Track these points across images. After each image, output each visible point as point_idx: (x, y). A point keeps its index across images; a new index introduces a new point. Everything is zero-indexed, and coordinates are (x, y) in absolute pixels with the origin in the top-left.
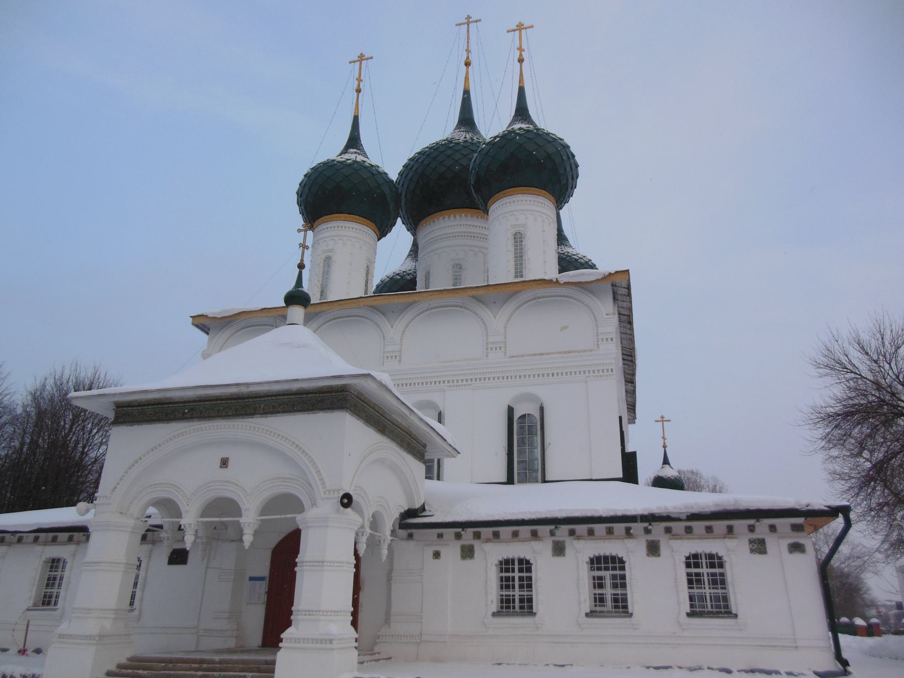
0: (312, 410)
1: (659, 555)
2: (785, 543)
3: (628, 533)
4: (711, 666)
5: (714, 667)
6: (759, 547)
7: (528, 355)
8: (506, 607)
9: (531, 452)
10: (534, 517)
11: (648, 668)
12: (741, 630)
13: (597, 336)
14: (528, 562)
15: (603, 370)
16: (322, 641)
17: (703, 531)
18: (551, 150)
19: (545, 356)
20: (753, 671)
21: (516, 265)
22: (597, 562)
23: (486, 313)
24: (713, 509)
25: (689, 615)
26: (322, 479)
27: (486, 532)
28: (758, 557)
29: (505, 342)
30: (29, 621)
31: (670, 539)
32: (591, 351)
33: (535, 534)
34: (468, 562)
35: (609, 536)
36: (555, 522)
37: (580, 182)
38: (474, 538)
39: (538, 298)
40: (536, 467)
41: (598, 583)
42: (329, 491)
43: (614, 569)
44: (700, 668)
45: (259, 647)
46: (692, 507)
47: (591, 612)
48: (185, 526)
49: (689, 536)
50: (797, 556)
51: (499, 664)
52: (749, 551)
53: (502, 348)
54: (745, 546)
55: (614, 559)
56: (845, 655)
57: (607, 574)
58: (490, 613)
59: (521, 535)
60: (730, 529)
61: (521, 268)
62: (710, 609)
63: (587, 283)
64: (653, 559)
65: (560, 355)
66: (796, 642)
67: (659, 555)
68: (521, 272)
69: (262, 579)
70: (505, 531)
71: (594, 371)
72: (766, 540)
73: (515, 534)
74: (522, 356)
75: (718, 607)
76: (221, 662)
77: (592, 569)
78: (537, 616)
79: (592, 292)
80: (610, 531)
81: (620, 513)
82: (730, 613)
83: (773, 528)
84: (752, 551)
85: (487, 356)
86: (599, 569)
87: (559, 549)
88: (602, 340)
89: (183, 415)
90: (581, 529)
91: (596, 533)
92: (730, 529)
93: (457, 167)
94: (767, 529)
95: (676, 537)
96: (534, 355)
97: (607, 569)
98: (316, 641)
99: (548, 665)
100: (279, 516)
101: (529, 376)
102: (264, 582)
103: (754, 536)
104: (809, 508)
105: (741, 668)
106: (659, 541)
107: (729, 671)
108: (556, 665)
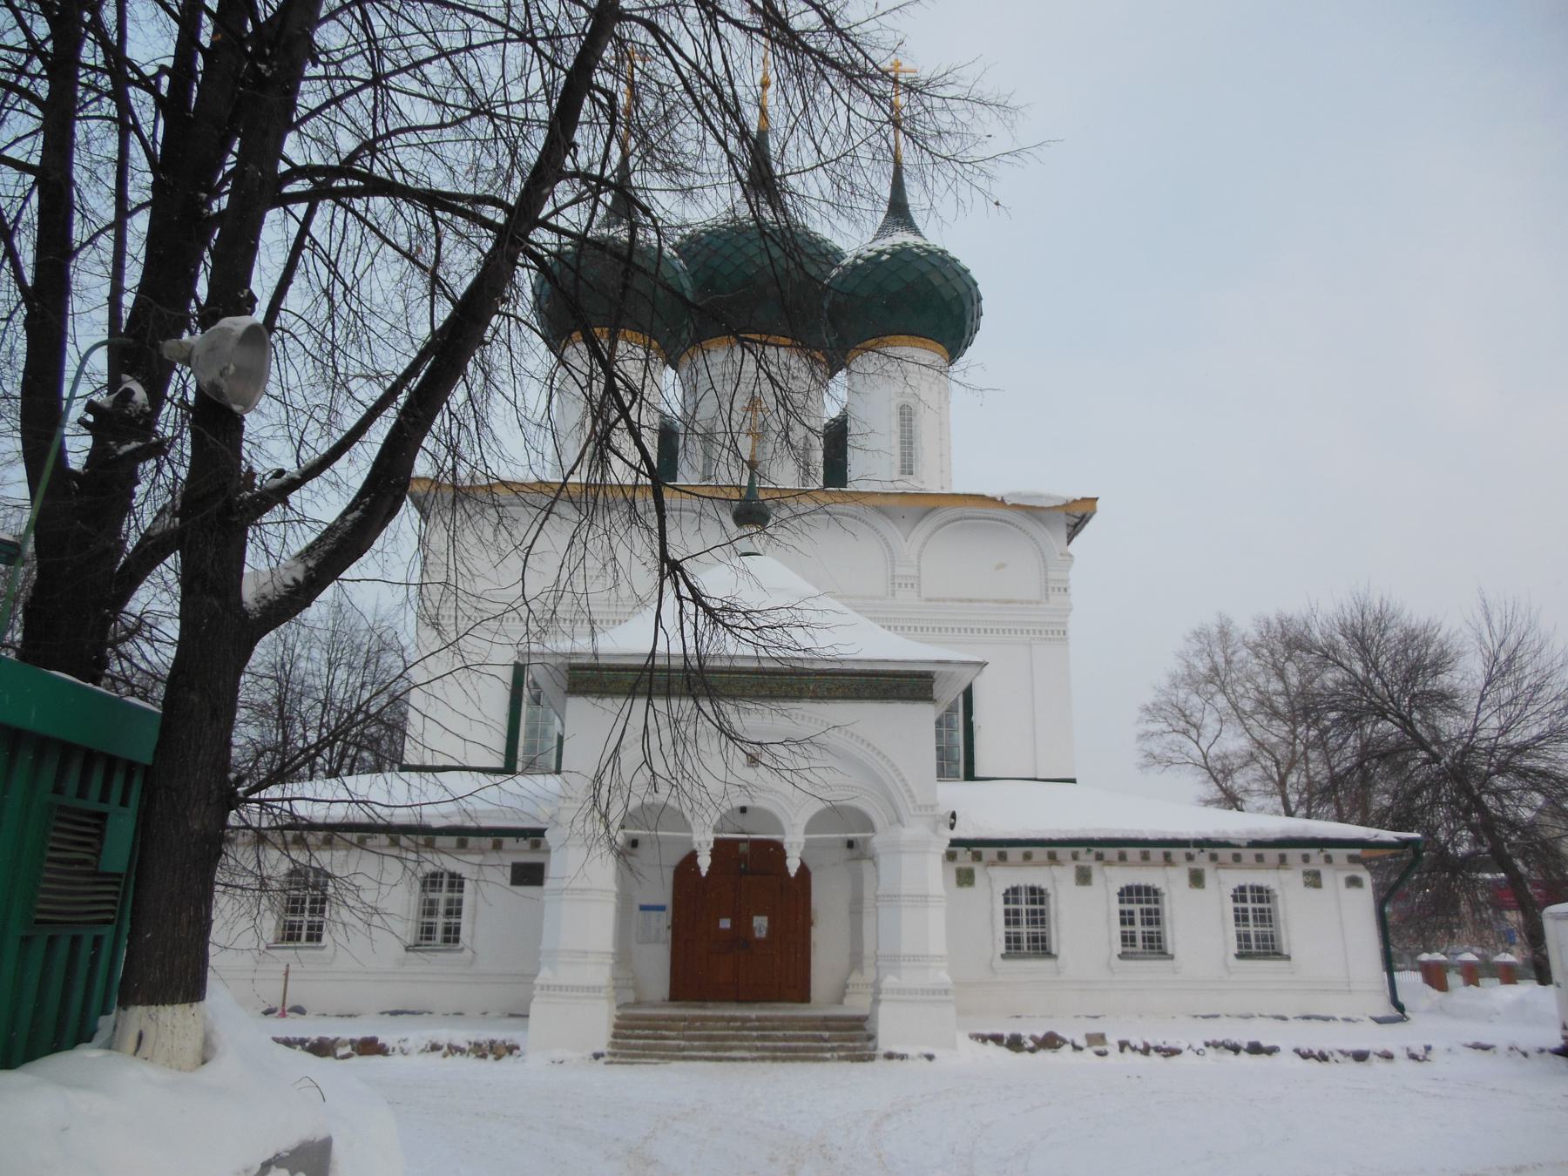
0: (887, 699)
1: (1203, 887)
2: (1342, 877)
3: (1168, 860)
4: (1262, 1013)
5: (1266, 1014)
6: (1314, 880)
7: (953, 600)
8: (1014, 946)
9: (950, 736)
10: (1063, 836)
11: (1195, 1017)
12: (1293, 973)
13: (1046, 582)
14: (1042, 892)
15: (1047, 631)
16: (934, 992)
17: (1252, 860)
18: (962, 289)
19: (977, 604)
20: (1307, 1018)
21: (903, 454)
22: (1128, 893)
23: (892, 532)
24: (1278, 836)
25: (1240, 956)
26: (909, 791)
27: (990, 853)
28: (1312, 892)
29: (919, 577)
30: (288, 965)
31: (1217, 868)
32: (1038, 603)
33: (1052, 858)
34: (966, 890)
35: (1145, 863)
36: (1088, 843)
37: (978, 337)
38: (973, 859)
39: (965, 519)
40: (957, 757)
41: (1126, 918)
42: (920, 807)
43: (1148, 902)
44: (1252, 1016)
45: (664, 1000)
46: (1256, 833)
47: (1124, 953)
48: (699, 845)
49: (1238, 865)
50: (1354, 891)
51: (1018, 1017)
52: (1302, 884)
53: (915, 586)
54: (1300, 879)
55: (1148, 890)
56: (1401, 998)
57: (1136, 908)
58: (998, 955)
59: (1035, 858)
60: (1283, 859)
61: (911, 461)
62: (1254, 949)
63: (1042, 508)
64: (1197, 892)
65: (997, 605)
66: (1349, 986)
67: (1203, 887)
68: (911, 466)
69: (661, 908)
70: (1015, 853)
71: (1040, 632)
72: (1322, 874)
73: (1027, 857)
74: (944, 600)
75: (1265, 947)
76: (759, 1019)
77: (1121, 902)
78: (1060, 958)
79: (1040, 519)
80: (1145, 857)
81: (1169, 837)
82: (1165, 953)
83: (1328, 859)
84: (1307, 884)
85: (893, 595)
86: (1131, 902)
87: (1084, 877)
88: (1053, 589)
89: (744, 690)
90: (1112, 853)
91: (1129, 858)
92: (1283, 859)
93: (249, 49)
94: (1322, 860)
95: (1223, 865)
96: (961, 600)
97: (1140, 902)
98: (924, 991)
99: (1078, 1016)
100: (837, 835)
101: (953, 629)
102: (663, 914)
103: (1308, 867)
104: (1378, 838)
105: (1297, 1015)
106: (1203, 870)
107: (1284, 1019)
108: (1088, 1017)
